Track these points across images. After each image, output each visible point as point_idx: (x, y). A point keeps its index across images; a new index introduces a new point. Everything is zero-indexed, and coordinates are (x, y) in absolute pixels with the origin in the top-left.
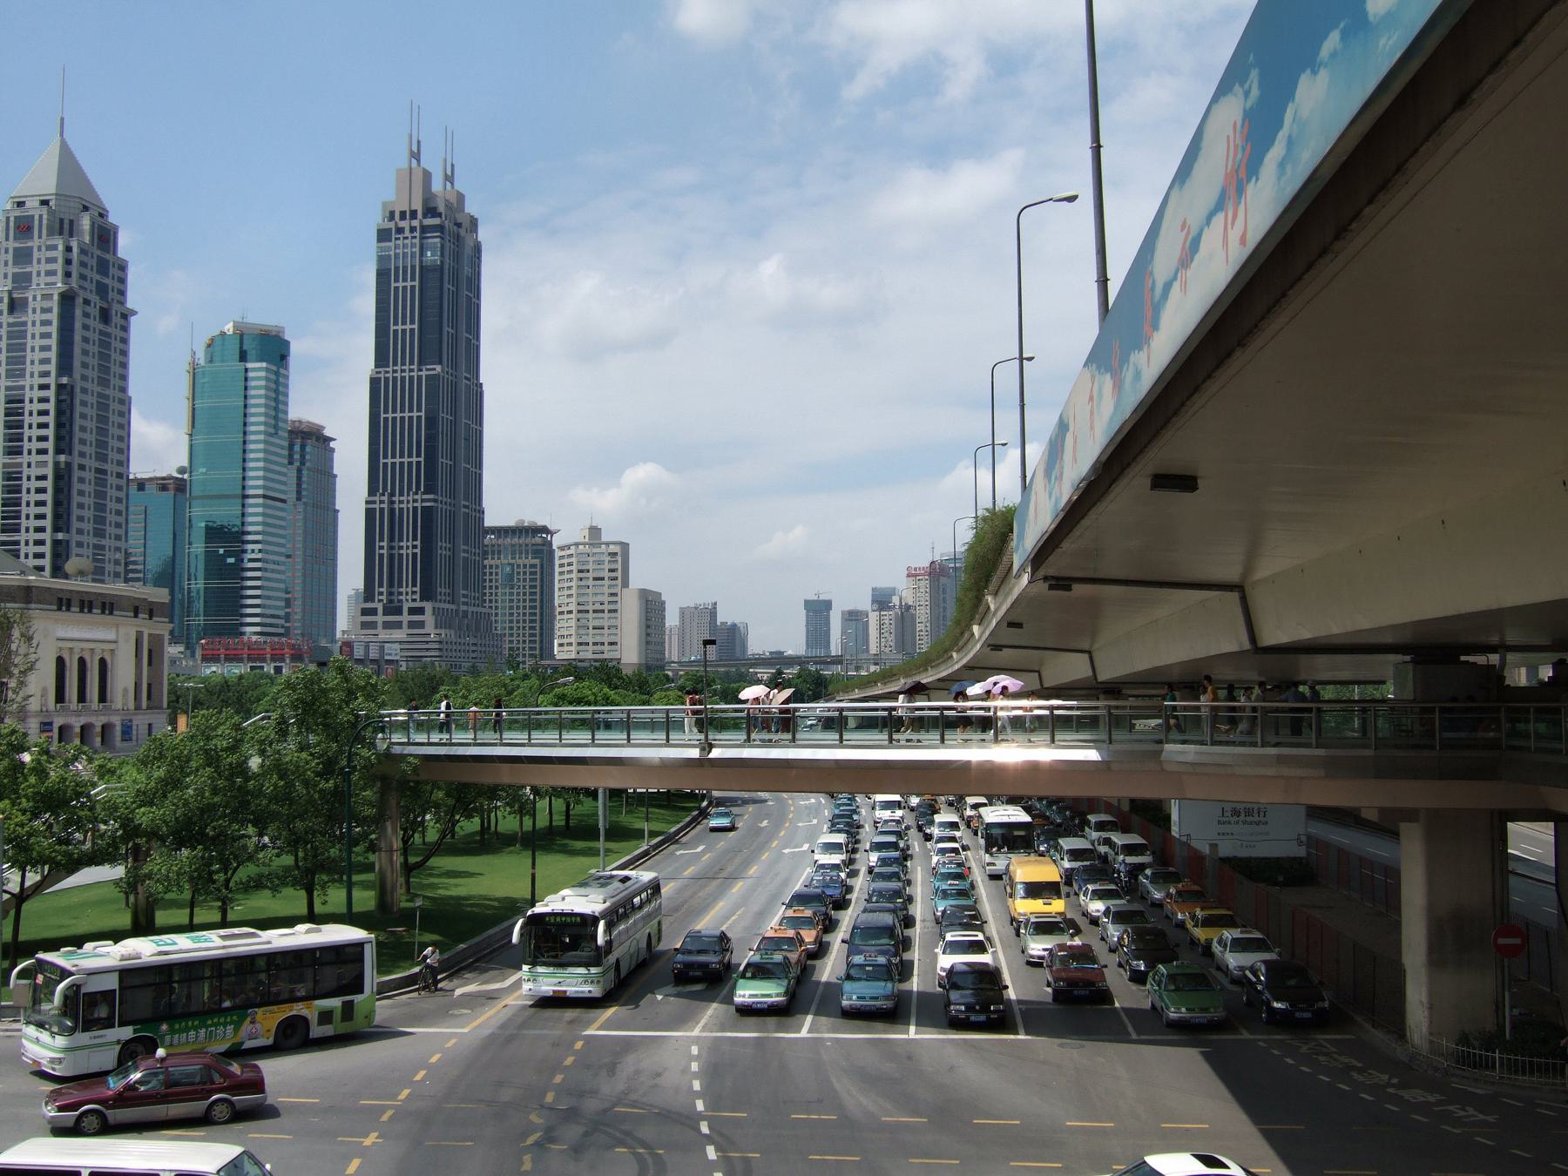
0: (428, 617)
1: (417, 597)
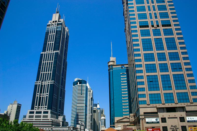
0: (49, 115)
1: (46, 109)
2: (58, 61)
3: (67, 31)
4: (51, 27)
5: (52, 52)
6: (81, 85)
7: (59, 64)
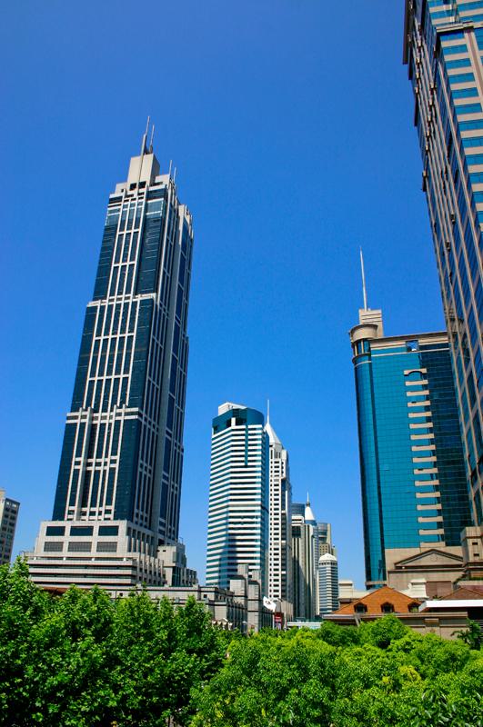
2: (154, 334)
3: (184, 219)
5: (128, 298)
6: (244, 427)
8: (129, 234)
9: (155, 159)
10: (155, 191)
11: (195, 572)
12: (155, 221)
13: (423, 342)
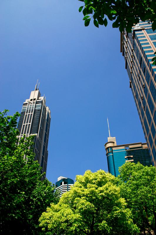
2: (36, 147)
3: (48, 111)
4: (28, 106)
5: (28, 135)
6: (67, 185)
7: (37, 151)
8: (27, 125)
9: (39, 91)
10: (39, 101)
11: (85, 26)
12: (38, 111)
13: (130, 147)
